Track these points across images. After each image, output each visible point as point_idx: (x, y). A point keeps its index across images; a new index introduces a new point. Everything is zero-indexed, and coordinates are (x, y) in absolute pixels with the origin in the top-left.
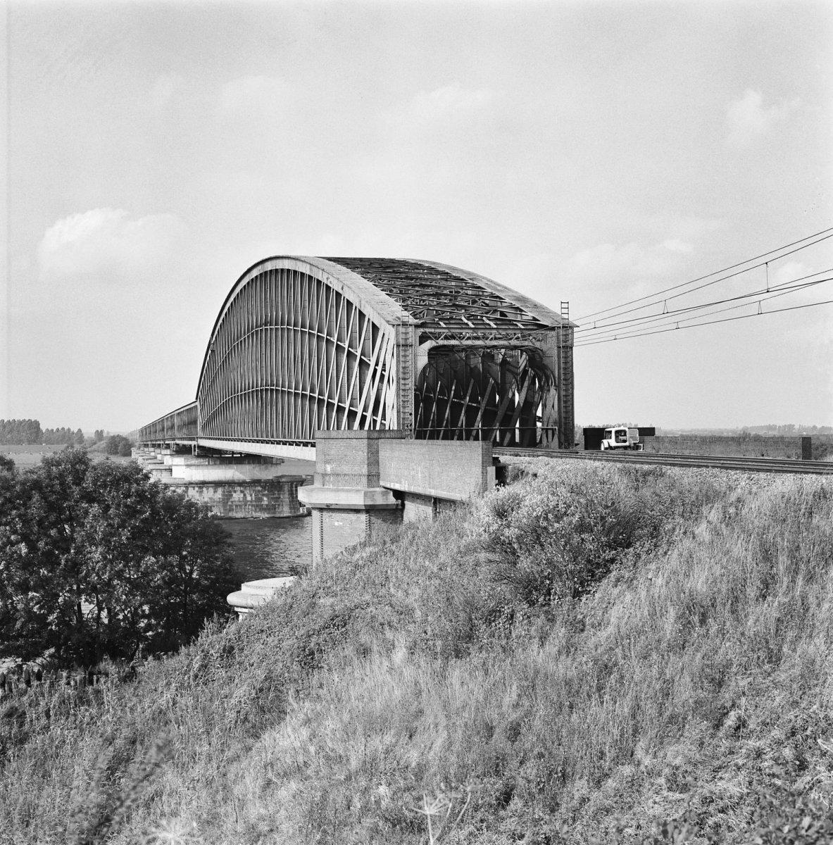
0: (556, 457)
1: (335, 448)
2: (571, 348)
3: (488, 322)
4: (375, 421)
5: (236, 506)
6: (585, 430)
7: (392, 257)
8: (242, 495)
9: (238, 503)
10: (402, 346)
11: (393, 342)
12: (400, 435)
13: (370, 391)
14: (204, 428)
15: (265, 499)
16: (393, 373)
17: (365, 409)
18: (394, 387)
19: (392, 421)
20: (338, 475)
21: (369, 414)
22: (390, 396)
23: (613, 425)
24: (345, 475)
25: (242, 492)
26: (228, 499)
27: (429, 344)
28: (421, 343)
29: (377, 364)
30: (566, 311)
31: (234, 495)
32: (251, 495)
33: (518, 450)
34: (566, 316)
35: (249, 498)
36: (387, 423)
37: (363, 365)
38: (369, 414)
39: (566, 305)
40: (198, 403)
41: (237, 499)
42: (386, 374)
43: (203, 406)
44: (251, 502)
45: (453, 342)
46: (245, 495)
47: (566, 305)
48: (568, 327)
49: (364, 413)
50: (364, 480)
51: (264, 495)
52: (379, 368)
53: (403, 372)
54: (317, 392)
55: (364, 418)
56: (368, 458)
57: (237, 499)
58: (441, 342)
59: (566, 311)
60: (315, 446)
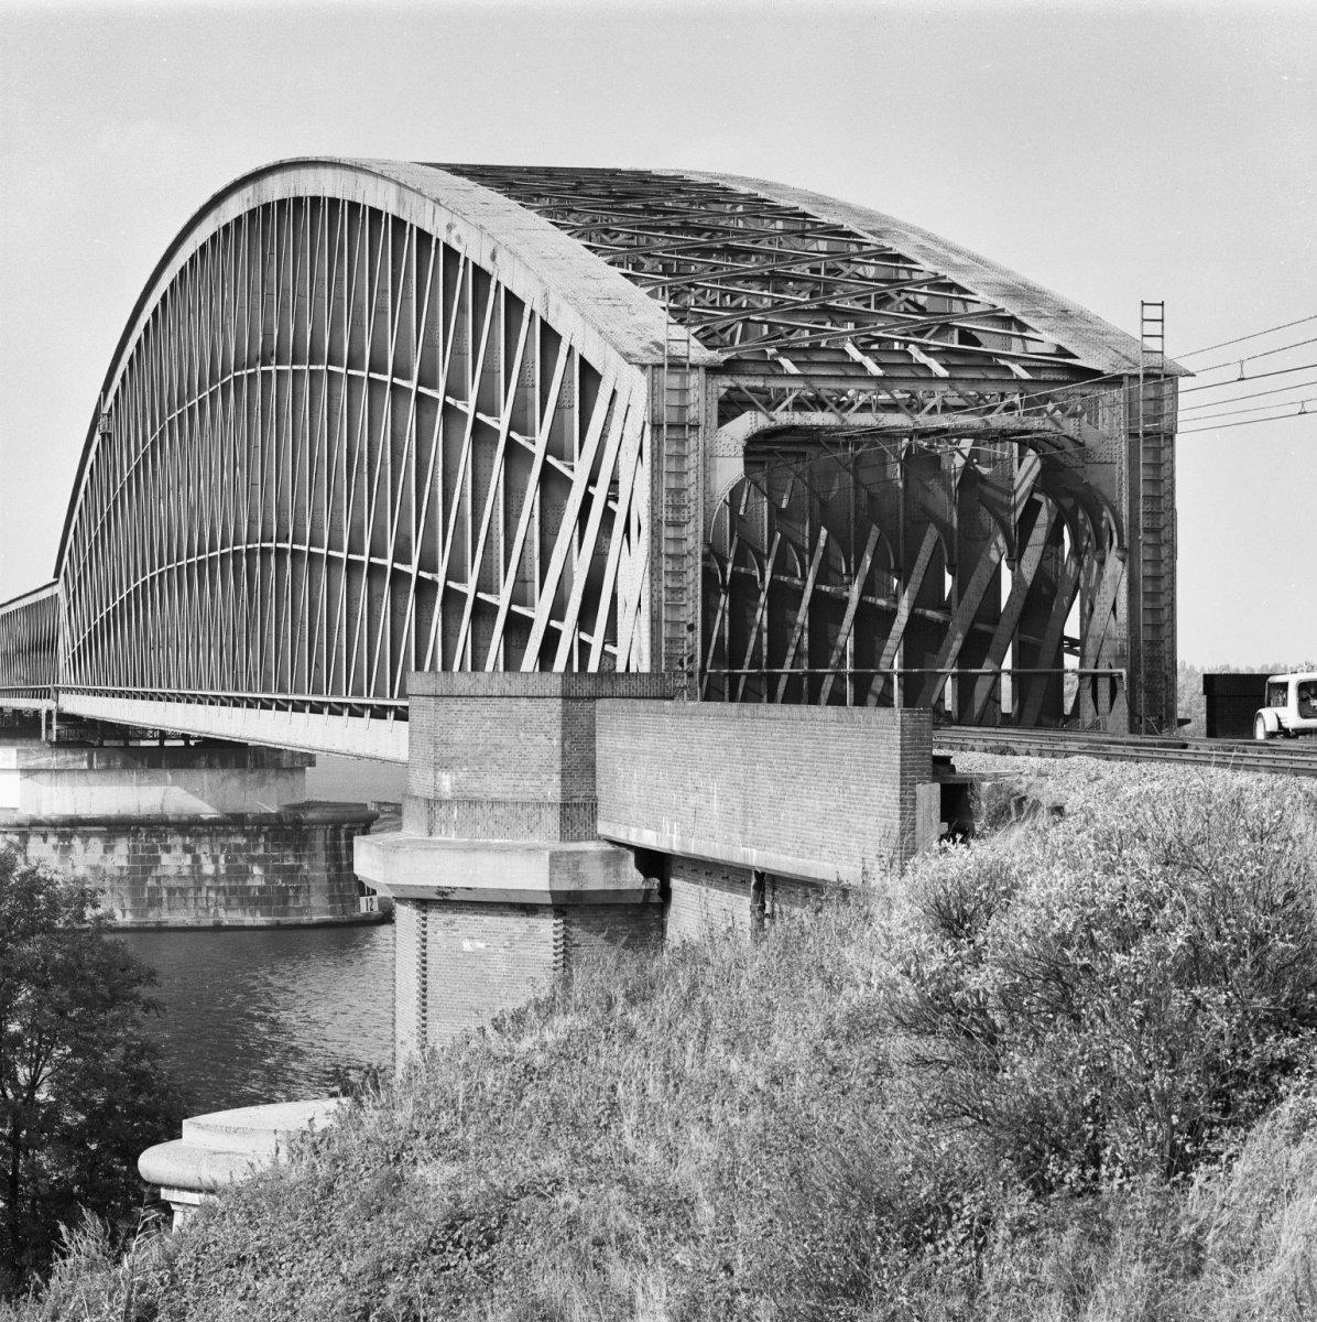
0: (1122, 758)
1: (469, 725)
2: (1171, 438)
3: (923, 359)
4: (585, 648)
5: (171, 891)
6: (1210, 681)
7: (641, 167)
8: (188, 860)
9: (174, 883)
10: (669, 428)
11: (640, 413)
12: (658, 687)
13: (571, 556)
14: (77, 659)
15: (257, 870)
16: (641, 509)
17: (558, 611)
18: (641, 546)
19: (634, 648)
20: (473, 803)
21: (568, 627)
22: (630, 572)
23: (1292, 665)
24: (494, 803)
25: (187, 849)
26: (147, 871)
27: (746, 424)
28: (724, 419)
29: (593, 481)
30: (1155, 328)
31: (165, 859)
32: (215, 860)
33: (1008, 736)
34: (1154, 344)
35: (208, 869)
36: (620, 651)
37: (553, 482)
38: (568, 627)
39: (1154, 312)
40: (59, 589)
41: (172, 871)
42: (620, 509)
43: (73, 597)
44: (215, 878)
45: (817, 418)
46: (196, 859)
47: (1154, 312)
48: (1161, 379)
49: (554, 623)
50: (552, 819)
51: (253, 860)
52: (600, 493)
53: (669, 507)
54: (415, 559)
55: (552, 637)
56: (564, 756)
57: (172, 871)
58: (783, 417)
59: (1155, 328)
60: (405, 718)
